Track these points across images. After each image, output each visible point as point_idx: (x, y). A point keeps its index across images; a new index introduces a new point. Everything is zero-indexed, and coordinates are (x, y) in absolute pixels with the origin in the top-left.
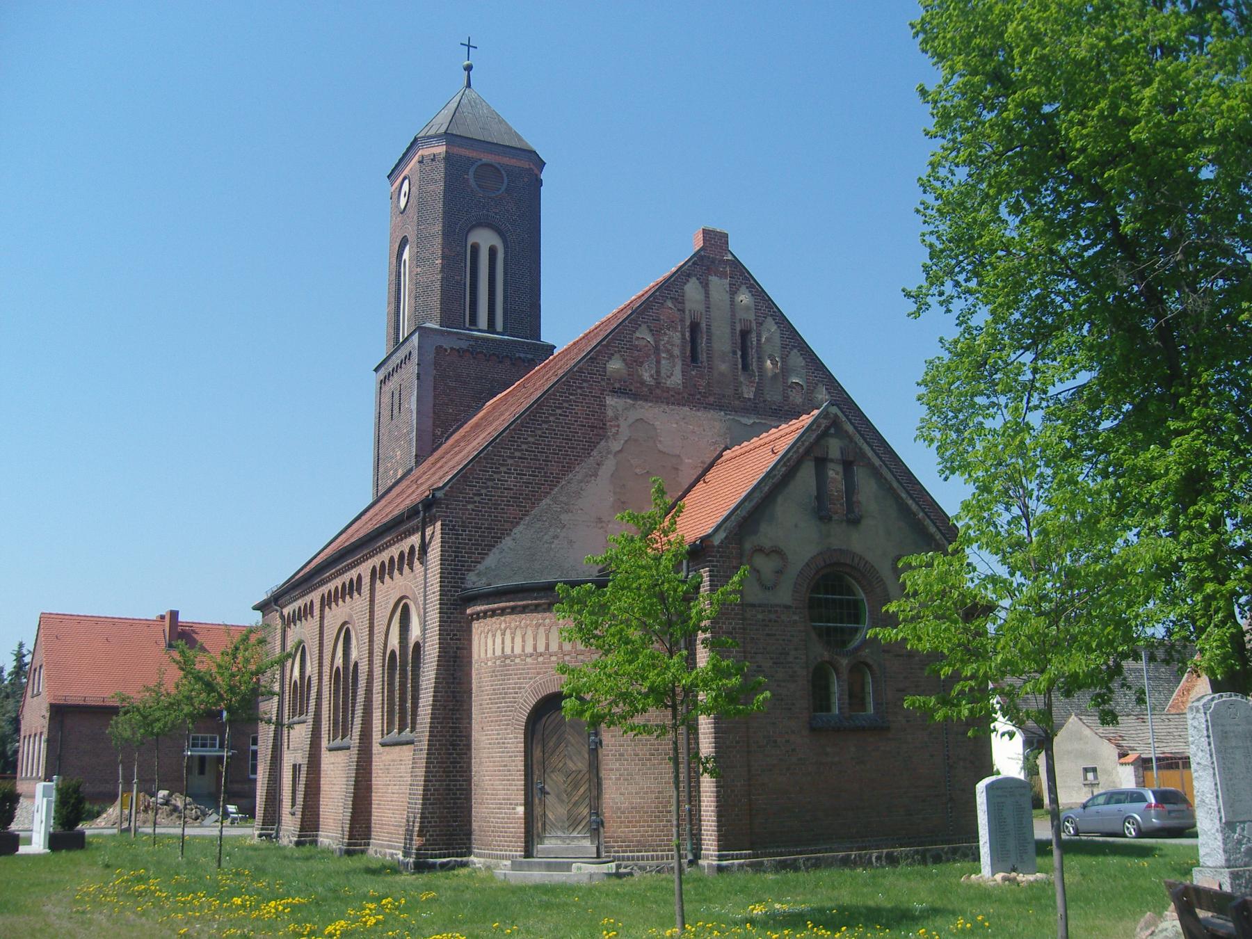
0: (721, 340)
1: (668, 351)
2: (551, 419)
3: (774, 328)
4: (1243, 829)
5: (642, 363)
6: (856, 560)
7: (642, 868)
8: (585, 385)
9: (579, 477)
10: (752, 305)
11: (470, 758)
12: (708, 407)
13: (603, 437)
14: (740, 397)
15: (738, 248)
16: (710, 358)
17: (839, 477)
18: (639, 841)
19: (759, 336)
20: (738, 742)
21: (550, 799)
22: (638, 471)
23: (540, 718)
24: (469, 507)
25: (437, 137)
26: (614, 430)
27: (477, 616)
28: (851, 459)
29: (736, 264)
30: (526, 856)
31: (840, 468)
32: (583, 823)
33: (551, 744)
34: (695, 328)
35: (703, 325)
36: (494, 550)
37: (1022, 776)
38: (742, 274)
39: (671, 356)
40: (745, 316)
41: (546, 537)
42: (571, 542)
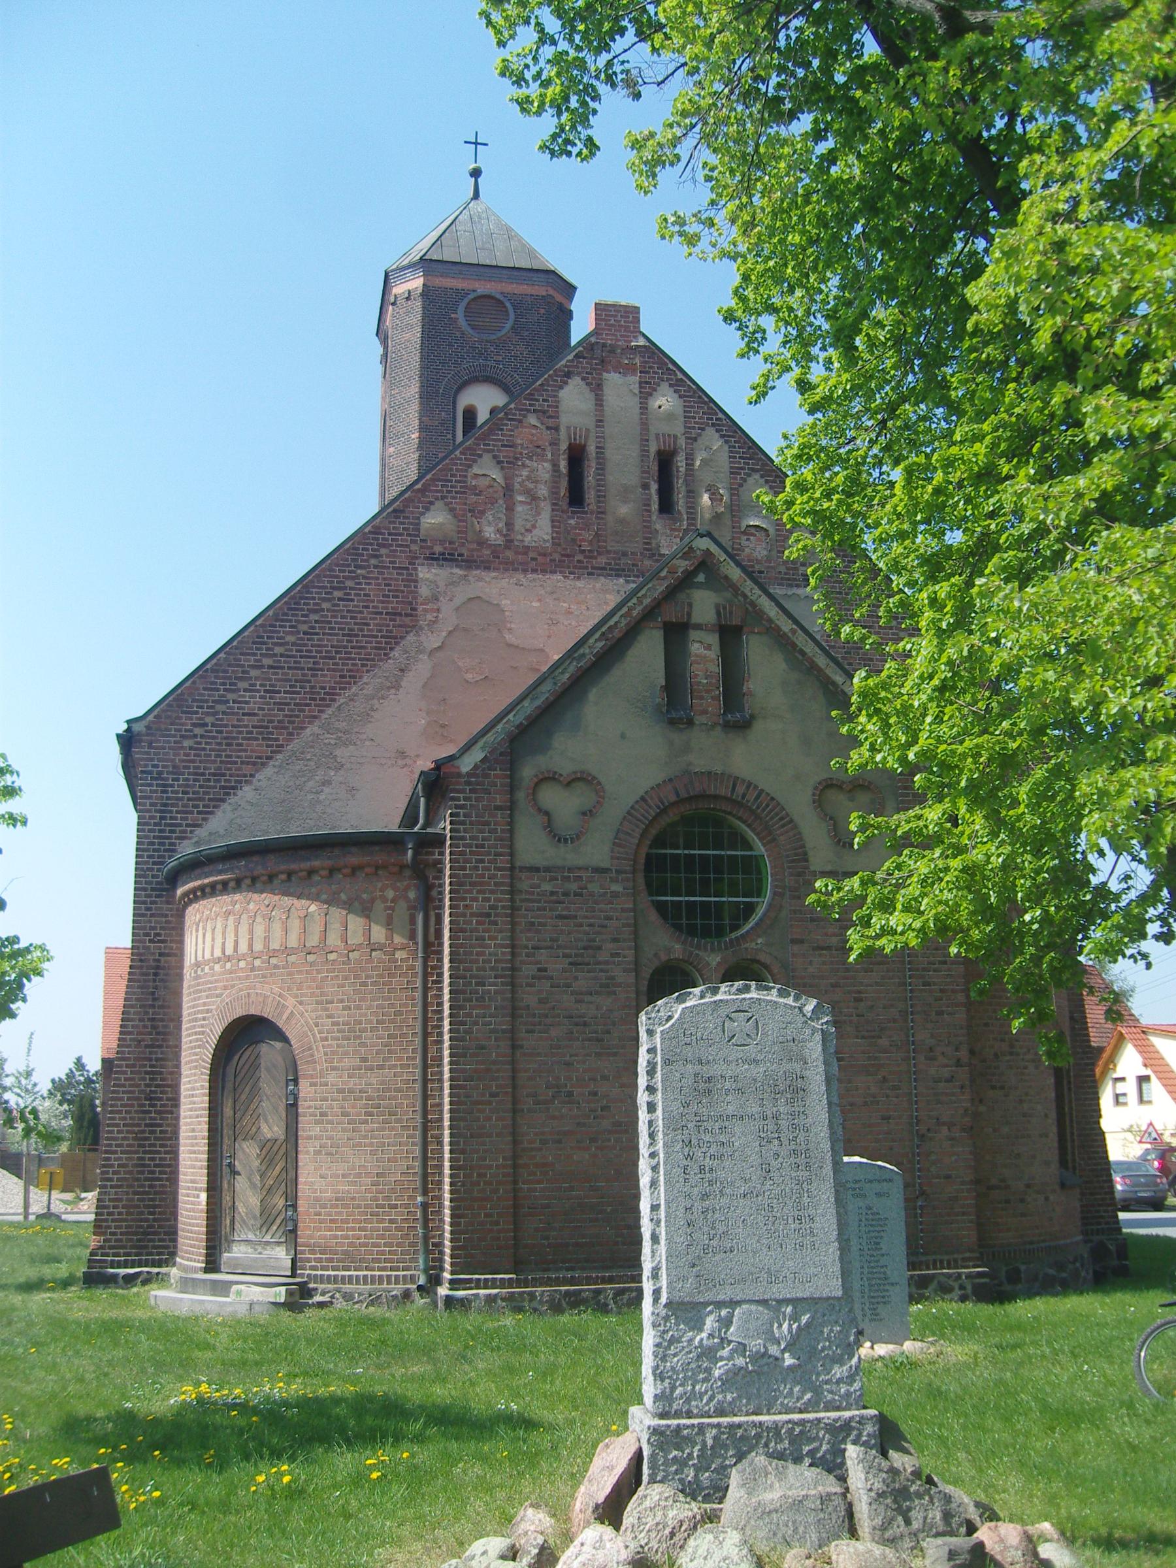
0: (622, 470)
1: (528, 492)
2: (325, 605)
3: (717, 444)
4: (727, 1322)
5: (483, 512)
6: (740, 790)
7: (348, 1297)
8: (383, 551)
9: (368, 690)
10: (679, 411)
11: (177, 1118)
12: (594, 572)
13: (414, 627)
14: (651, 552)
15: (652, 327)
16: (601, 497)
17: (713, 654)
18: (346, 1253)
19: (690, 459)
20: (492, 1095)
21: (241, 1183)
22: (469, 676)
23: (229, 1059)
24: (186, 743)
25: (411, 266)
26: (430, 617)
27: (196, 896)
28: (736, 621)
29: (653, 352)
30: (207, 1270)
31: (713, 639)
32: (278, 1221)
33: (243, 1097)
34: (576, 457)
35: (591, 449)
36: (225, 806)
37: (91, 1196)
38: (662, 364)
39: (534, 498)
40: (665, 428)
41: (311, 783)
42: (352, 790)
